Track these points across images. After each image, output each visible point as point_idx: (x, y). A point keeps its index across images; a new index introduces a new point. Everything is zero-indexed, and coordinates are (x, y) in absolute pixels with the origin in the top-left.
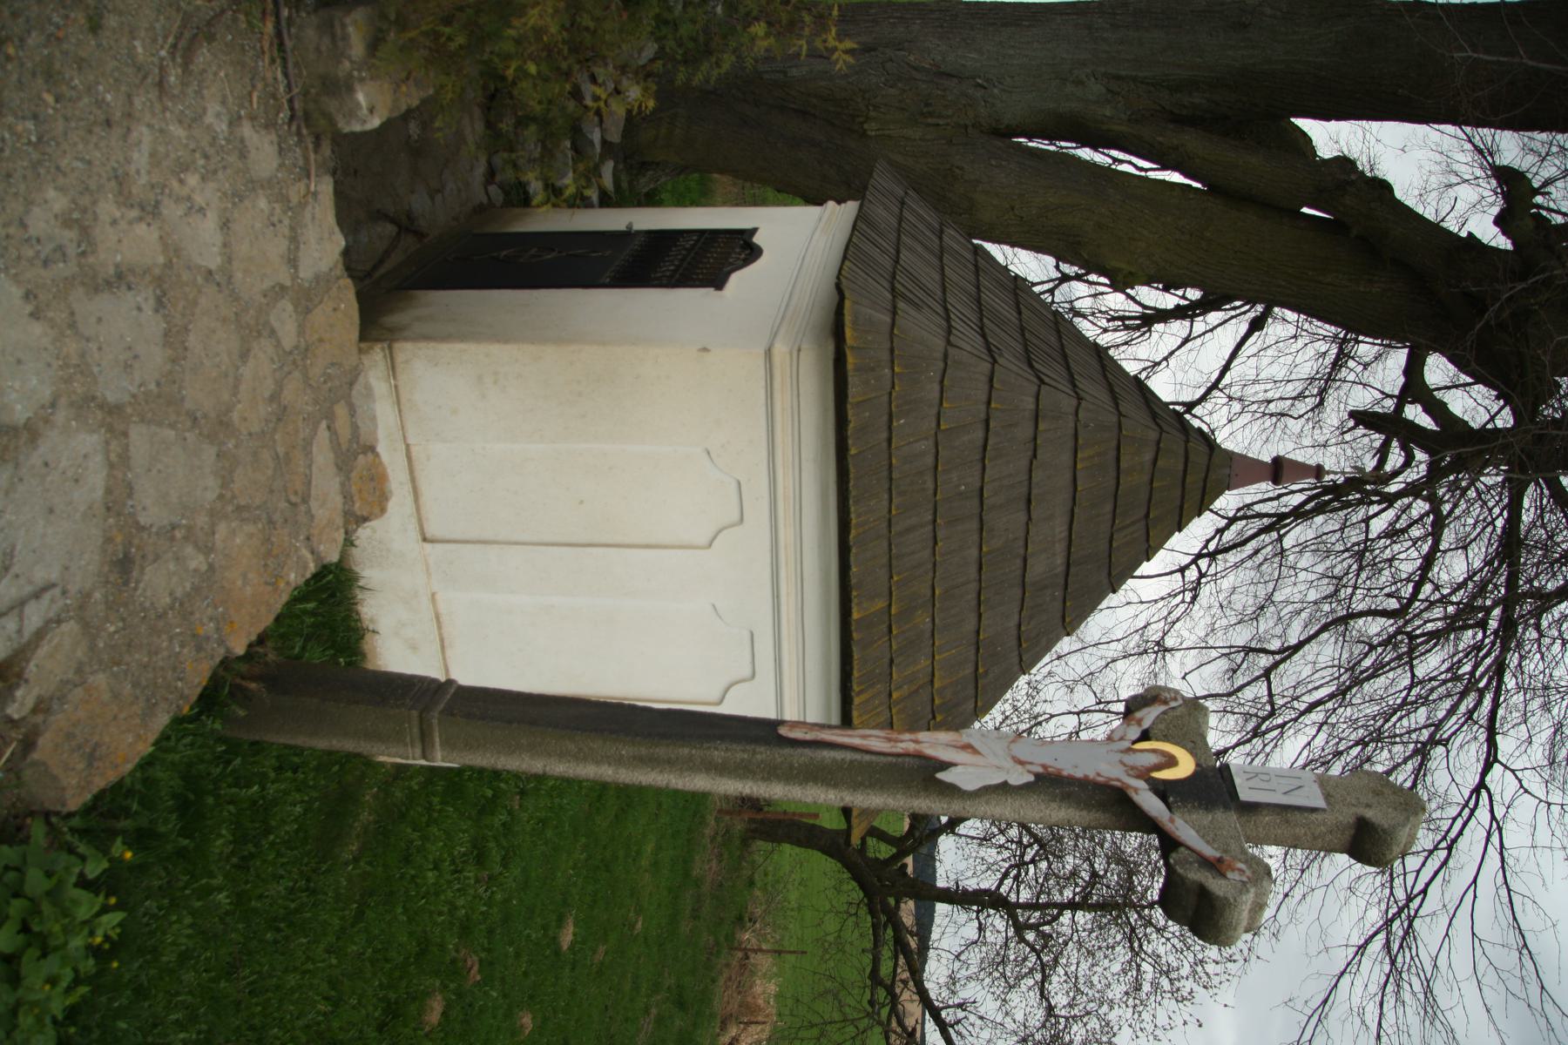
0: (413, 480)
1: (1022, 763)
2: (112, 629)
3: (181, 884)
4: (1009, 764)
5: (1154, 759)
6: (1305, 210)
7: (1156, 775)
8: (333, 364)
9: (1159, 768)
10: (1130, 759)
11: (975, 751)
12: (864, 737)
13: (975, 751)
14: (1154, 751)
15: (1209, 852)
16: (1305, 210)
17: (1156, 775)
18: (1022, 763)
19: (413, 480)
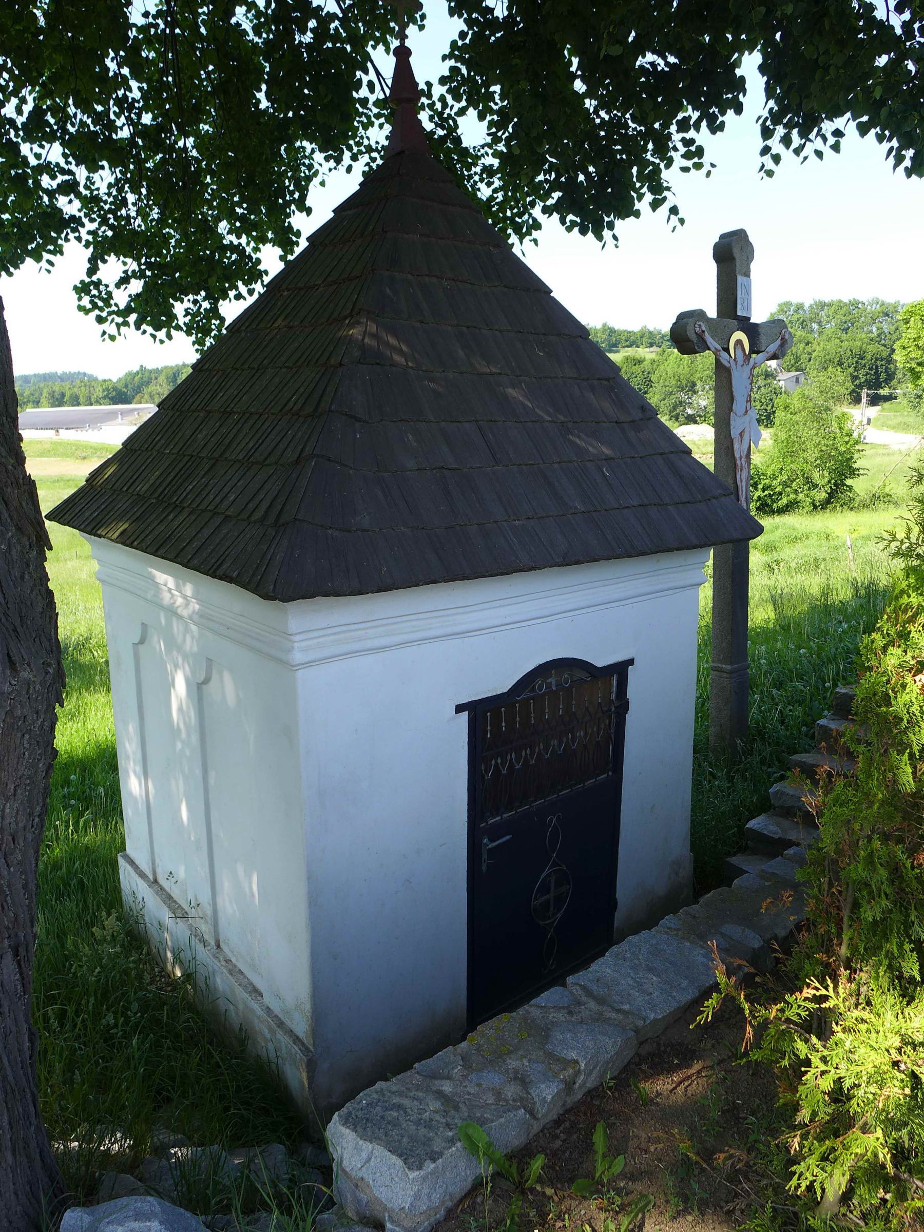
0: (161, 545)
1: (747, 411)
2: (308, 38)
3: (810, 892)
4: (747, 418)
5: (739, 351)
6: (508, 837)
7: (747, 352)
8: (641, 1043)
9: (744, 350)
10: (740, 362)
11: (743, 431)
12: (741, 481)
13: (743, 431)
14: (735, 349)
15: (778, 342)
16: (508, 837)
17: (747, 352)
18: (747, 411)
19: (161, 545)
